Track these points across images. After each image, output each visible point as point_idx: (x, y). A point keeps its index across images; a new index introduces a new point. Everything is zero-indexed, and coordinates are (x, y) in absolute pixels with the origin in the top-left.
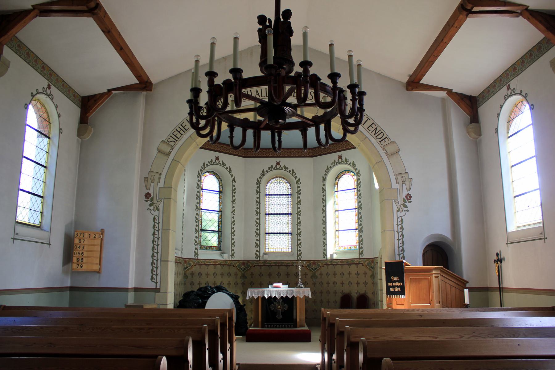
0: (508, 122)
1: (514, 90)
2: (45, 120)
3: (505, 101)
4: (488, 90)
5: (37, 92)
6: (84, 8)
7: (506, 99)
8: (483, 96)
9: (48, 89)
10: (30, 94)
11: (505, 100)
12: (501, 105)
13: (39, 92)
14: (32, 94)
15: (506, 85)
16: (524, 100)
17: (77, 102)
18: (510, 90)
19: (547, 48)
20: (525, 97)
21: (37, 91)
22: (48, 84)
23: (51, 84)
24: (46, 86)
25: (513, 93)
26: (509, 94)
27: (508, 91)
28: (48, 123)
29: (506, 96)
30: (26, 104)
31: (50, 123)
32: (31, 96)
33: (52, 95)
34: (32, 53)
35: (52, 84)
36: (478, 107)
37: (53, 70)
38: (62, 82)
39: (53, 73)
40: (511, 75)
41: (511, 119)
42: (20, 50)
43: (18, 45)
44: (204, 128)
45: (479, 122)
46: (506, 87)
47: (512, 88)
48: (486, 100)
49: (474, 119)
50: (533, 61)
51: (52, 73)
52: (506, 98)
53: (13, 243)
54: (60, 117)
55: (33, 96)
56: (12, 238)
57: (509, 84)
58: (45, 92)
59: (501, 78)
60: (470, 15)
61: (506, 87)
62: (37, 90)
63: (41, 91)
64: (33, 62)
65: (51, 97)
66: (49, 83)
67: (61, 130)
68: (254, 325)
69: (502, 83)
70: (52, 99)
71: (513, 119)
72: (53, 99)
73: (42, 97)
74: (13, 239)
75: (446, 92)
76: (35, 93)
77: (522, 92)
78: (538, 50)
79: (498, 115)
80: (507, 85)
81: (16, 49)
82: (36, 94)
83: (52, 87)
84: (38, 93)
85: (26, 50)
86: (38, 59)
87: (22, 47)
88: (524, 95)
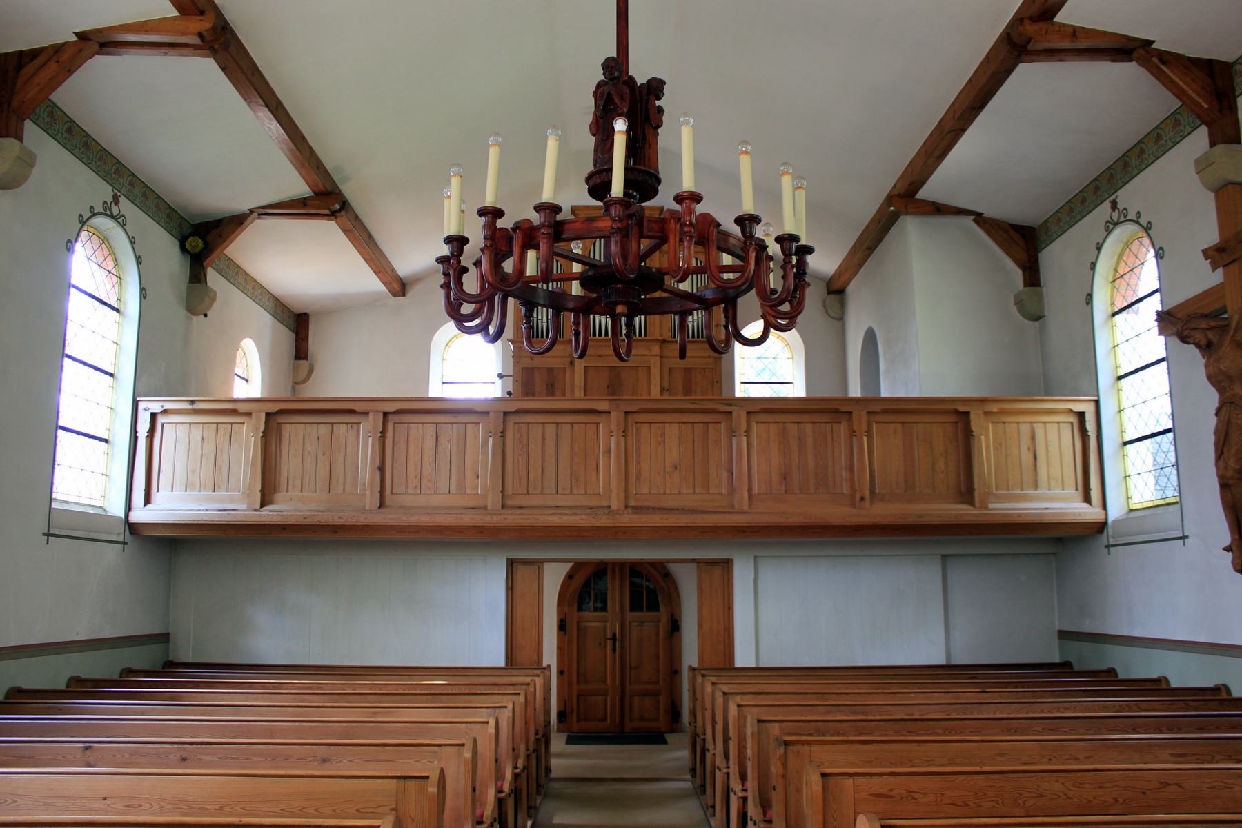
0: (1112, 282)
1: (1125, 211)
2: (110, 272)
3: (1108, 234)
4: (1158, 134)
5: (91, 212)
6: (327, 212)
7: (1109, 232)
8: (1048, 229)
9: (113, 204)
10: (77, 219)
11: (1106, 233)
12: (1098, 243)
13: (95, 212)
14: (81, 218)
15: (1107, 198)
16: (1145, 235)
17: (164, 219)
18: (1117, 211)
19: (1192, 123)
20: (1147, 229)
21: (90, 211)
22: (112, 193)
23: (119, 194)
24: (110, 200)
25: (1122, 219)
26: (1115, 220)
27: (1113, 213)
28: (115, 279)
29: (1108, 224)
30: (69, 241)
31: (121, 279)
32: (78, 222)
33: (123, 216)
34: (93, 143)
35: (120, 192)
36: (1237, 94)
37: (107, 151)
38: (156, 198)
39: (109, 157)
40: (1168, 138)
41: (1118, 276)
42: (71, 139)
43: (100, 157)
44: (471, 317)
45: (1042, 284)
46: (1107, 205)
47: (1121, 206)
48: (1065, 229)
49: (1032, 276)
50: (1181, 136)
51: (106, 156)
52: (1108, 227)
53: (46, 543)
54: (140, 263)
55: (83, 222)
56: (44, 534)
57: (1114, 197)
58: (108, 212)
59: (1142, 145)
60: (1023, 57)
61: (1107, 205)
62: (92, 207)
63: (99, 209)
64: (81, 146)
65: (120, 220)
66: (115, 191)
67: (144, 292)
68: (665, 297)
69: (1162, 144)
70: (123, 225)
71: (1121, 277)
72: (125, 225)
73: (102, 222)
74: (48, 535)
75: (973, 217)
76: (87, 214)
77: (1140, 215)
78: (1173, 128)
79: (1093, 266)
80: (1111, 199)
81: (46, 121)
82: (89, 218)
83: (122, 199)
84: (94, 214)
85: (98, 152)
86: (75, 125)
87: (74, 133)
88: (1145, 225)
